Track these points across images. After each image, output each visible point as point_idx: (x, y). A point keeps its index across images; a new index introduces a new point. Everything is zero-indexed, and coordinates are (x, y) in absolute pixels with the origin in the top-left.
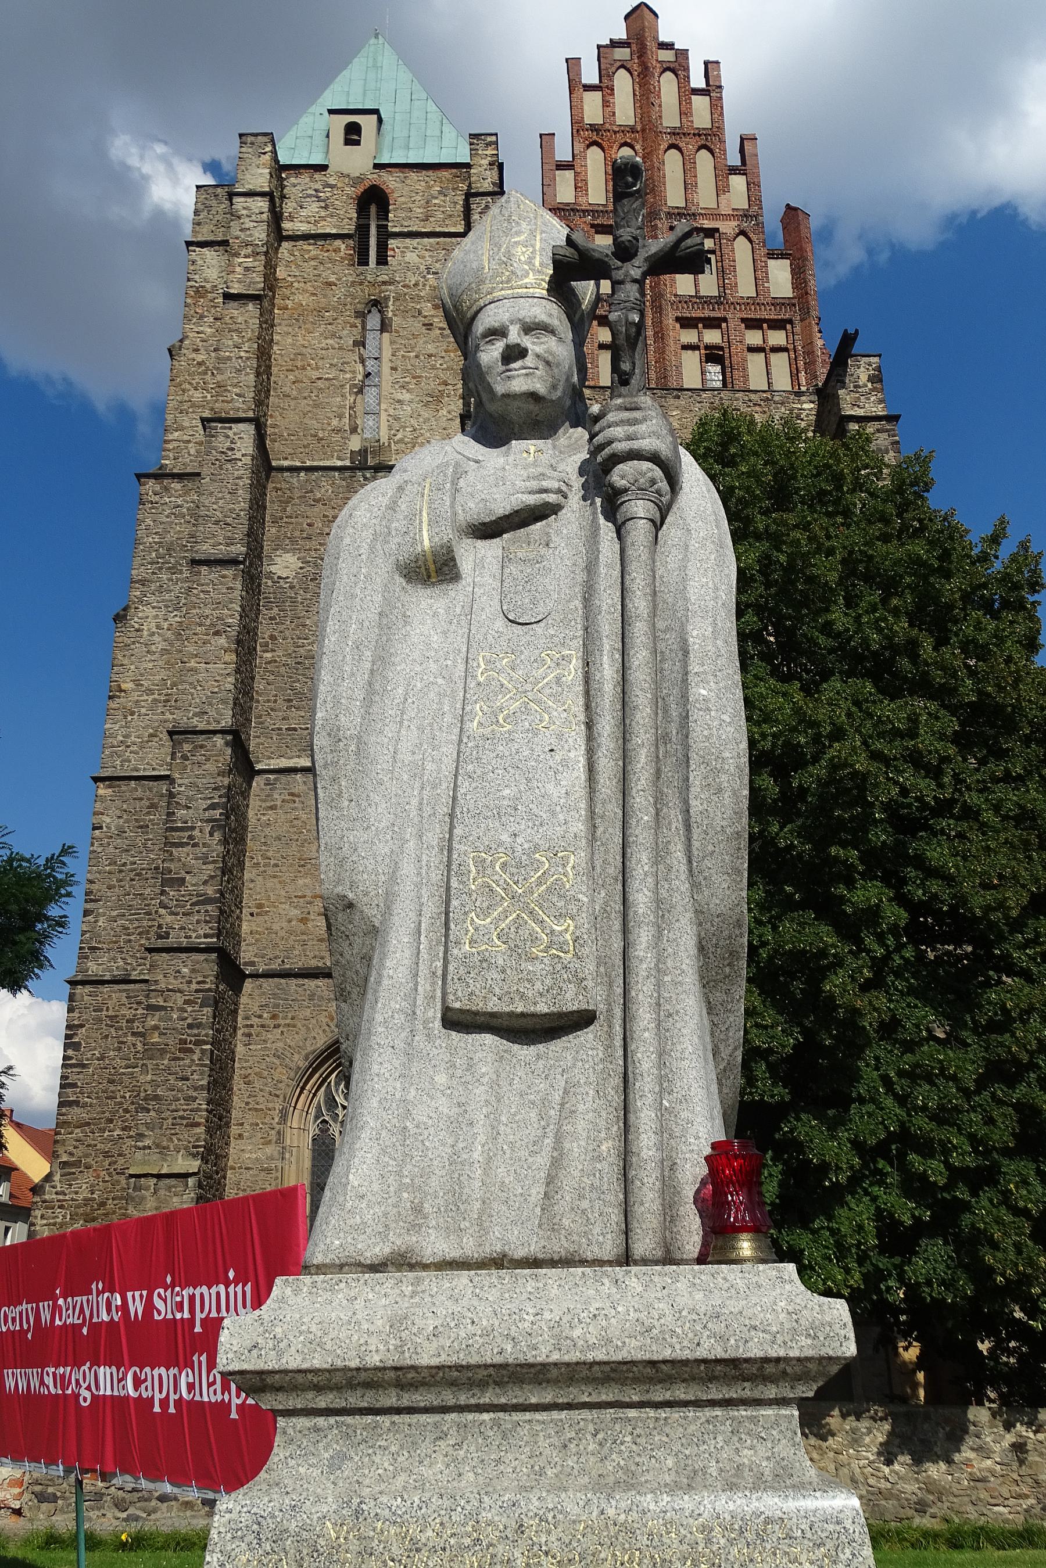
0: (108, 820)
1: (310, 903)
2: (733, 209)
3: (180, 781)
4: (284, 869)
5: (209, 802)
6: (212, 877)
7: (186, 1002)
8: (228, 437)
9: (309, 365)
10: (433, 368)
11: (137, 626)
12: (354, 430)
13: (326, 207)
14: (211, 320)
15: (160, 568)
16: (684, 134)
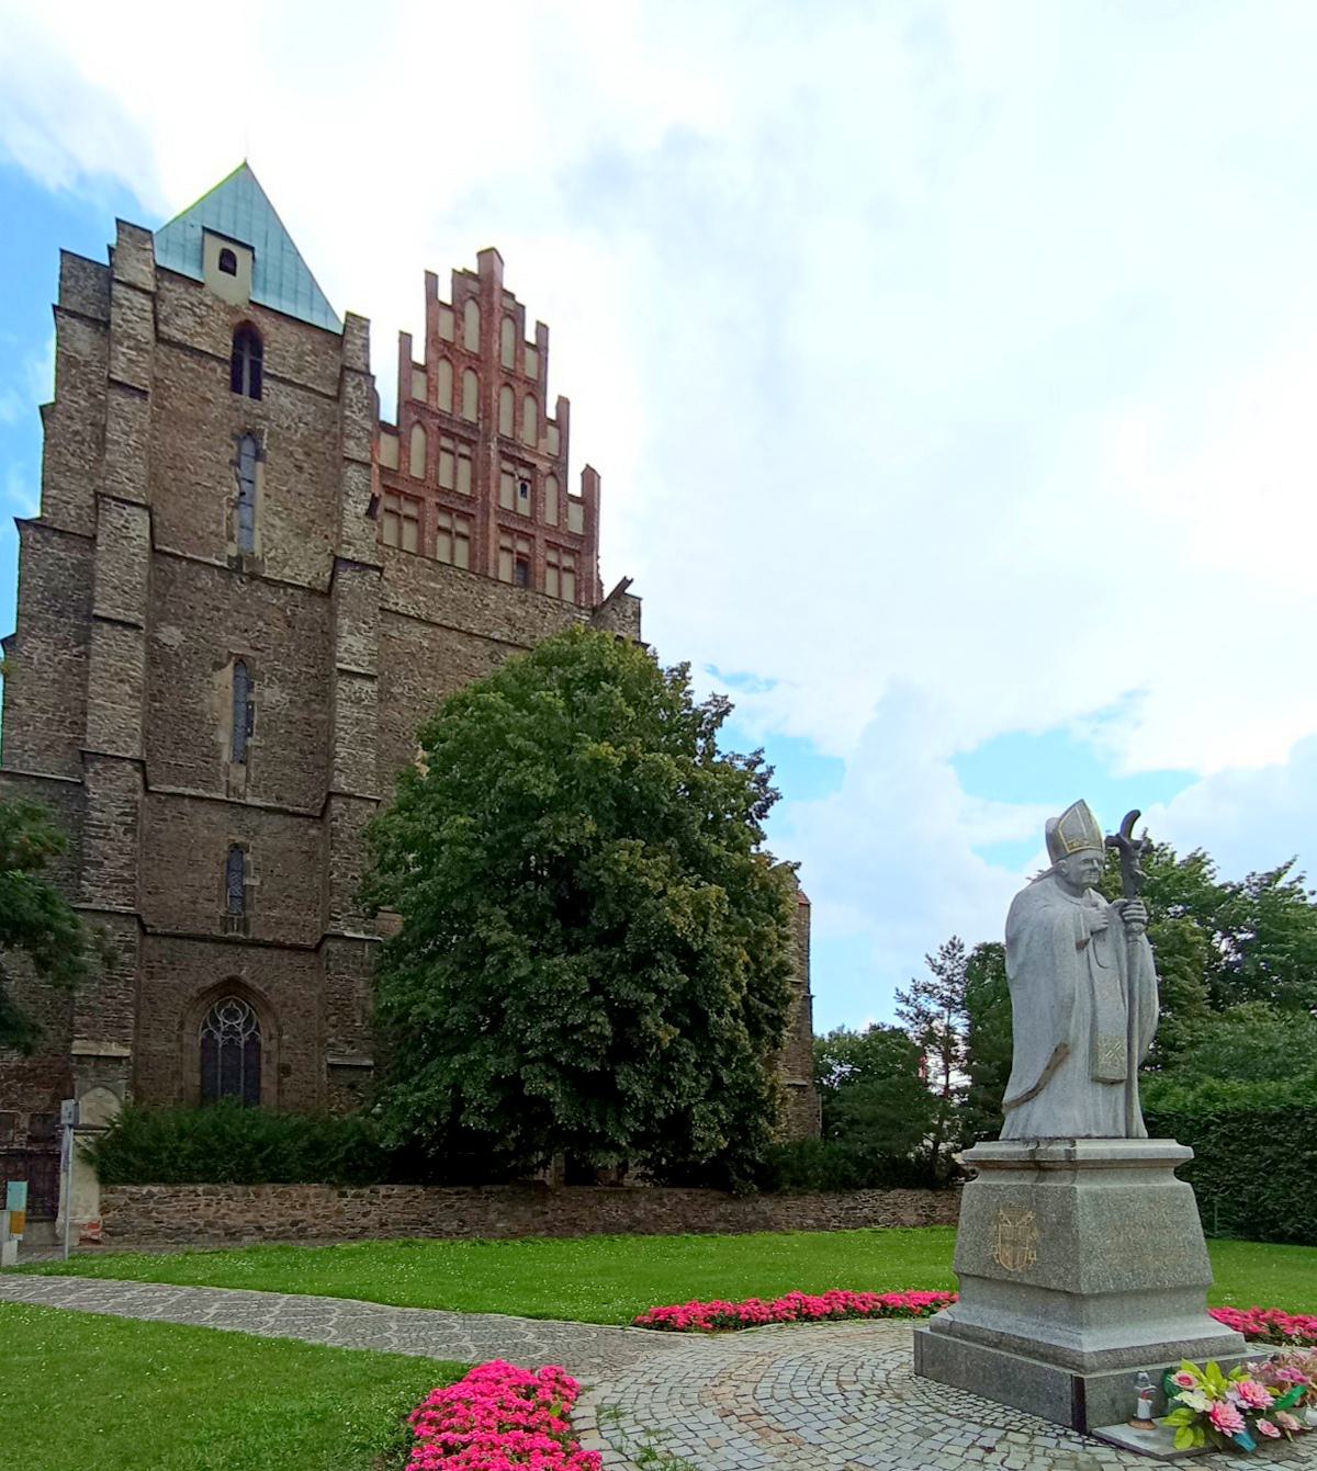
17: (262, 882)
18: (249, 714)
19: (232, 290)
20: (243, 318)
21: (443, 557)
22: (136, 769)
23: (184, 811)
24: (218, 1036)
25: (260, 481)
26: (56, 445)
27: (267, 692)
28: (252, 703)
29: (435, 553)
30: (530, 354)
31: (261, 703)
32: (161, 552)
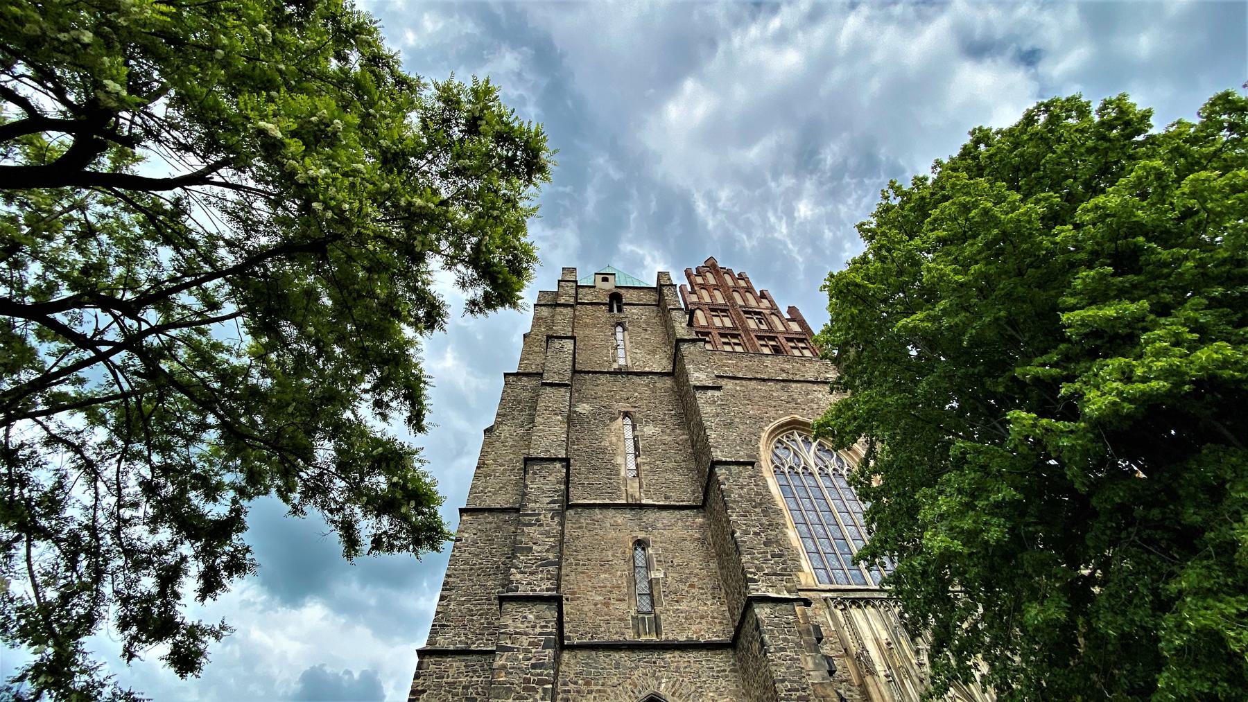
0: (467, 535)
4: (590, 567)
6: (552, 547)
12: (615, 361)
17: (665, 574)
19: (609, 286)
28: (637, 436)
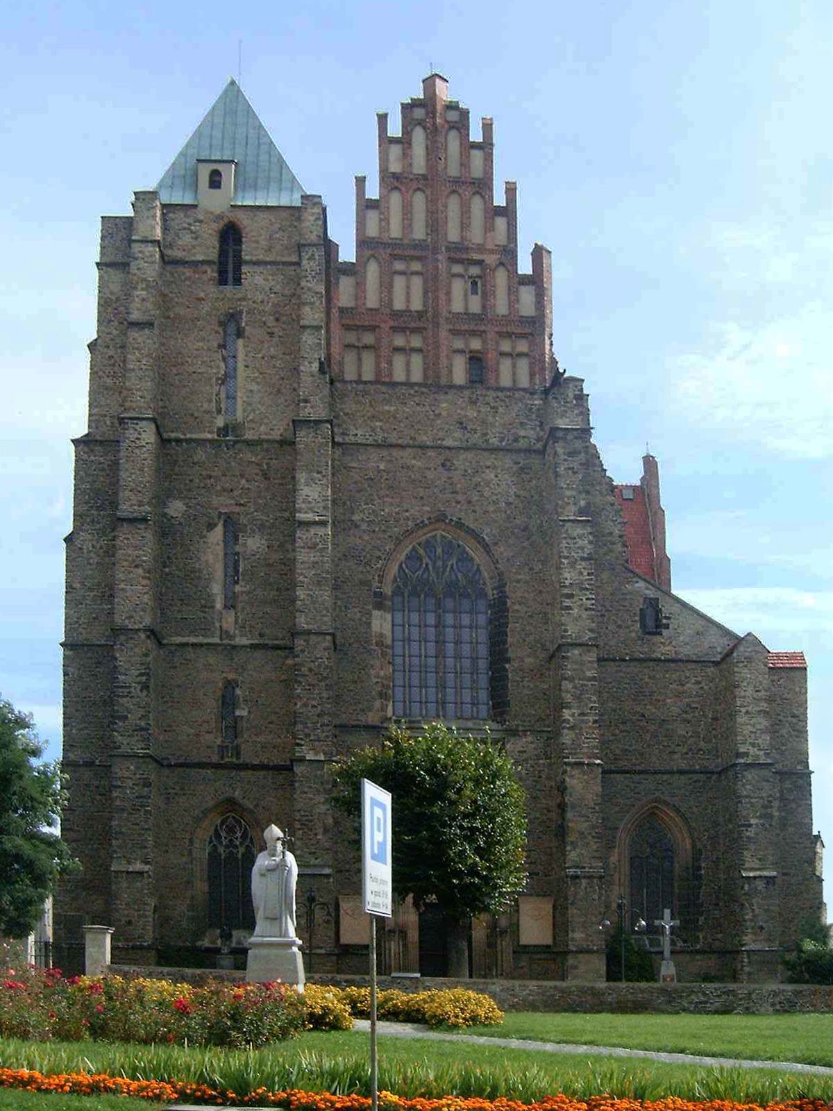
1: (201, 725)
2: (496, 246)
3: (120, 659)
5: (138, 672)
7: (134, 784)
8: (136, 430)
9: (187, 362)
10: (274, 366)
11: (79, 546)
13: (196, 238)
14: (116, 323)
15: (92, 507)
16: (463, 183)
17: (249, 712)
18: (236, 563)
19: (215, 202)
20: (226, 220)
21: (399, 376)
22: (148, 637)
23: (188, 657)
24: (221, 850)
25: (241, 356)
26: (96, 373)
27: (250, 542)
28: (237, 554)
29: (391, 375)
30: (477, 155)
31: (245, 552)
32: (169, 441)
